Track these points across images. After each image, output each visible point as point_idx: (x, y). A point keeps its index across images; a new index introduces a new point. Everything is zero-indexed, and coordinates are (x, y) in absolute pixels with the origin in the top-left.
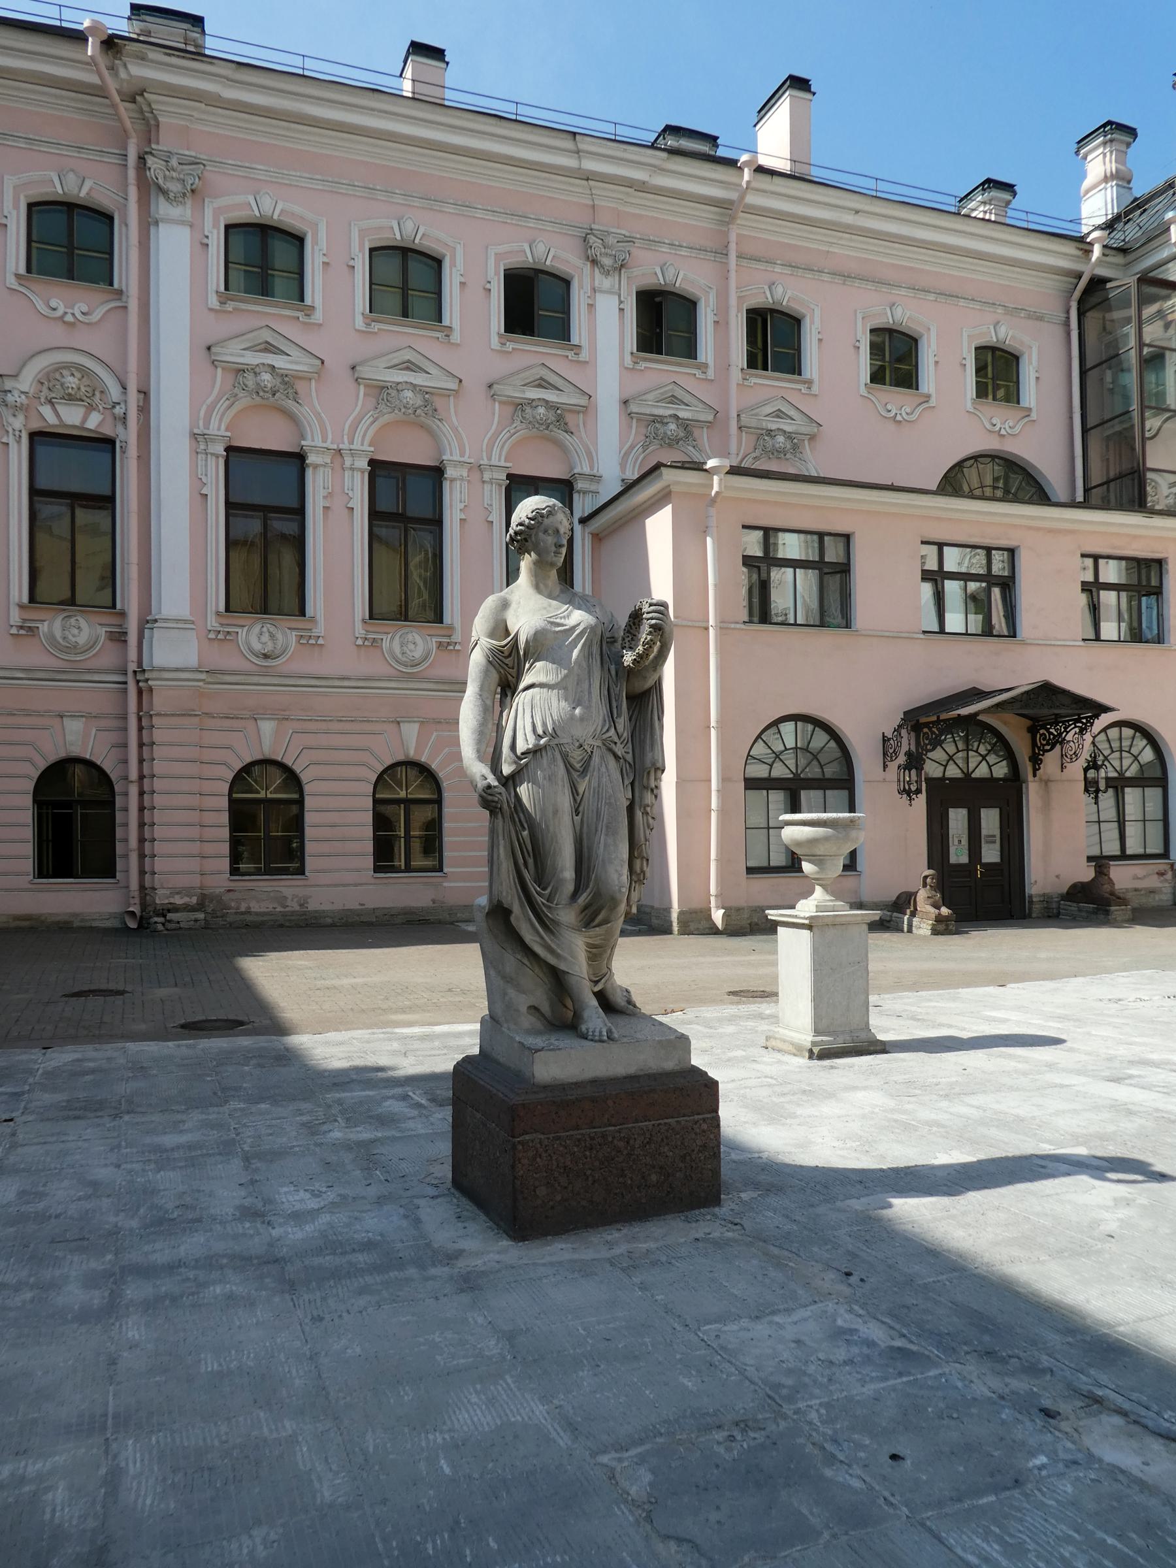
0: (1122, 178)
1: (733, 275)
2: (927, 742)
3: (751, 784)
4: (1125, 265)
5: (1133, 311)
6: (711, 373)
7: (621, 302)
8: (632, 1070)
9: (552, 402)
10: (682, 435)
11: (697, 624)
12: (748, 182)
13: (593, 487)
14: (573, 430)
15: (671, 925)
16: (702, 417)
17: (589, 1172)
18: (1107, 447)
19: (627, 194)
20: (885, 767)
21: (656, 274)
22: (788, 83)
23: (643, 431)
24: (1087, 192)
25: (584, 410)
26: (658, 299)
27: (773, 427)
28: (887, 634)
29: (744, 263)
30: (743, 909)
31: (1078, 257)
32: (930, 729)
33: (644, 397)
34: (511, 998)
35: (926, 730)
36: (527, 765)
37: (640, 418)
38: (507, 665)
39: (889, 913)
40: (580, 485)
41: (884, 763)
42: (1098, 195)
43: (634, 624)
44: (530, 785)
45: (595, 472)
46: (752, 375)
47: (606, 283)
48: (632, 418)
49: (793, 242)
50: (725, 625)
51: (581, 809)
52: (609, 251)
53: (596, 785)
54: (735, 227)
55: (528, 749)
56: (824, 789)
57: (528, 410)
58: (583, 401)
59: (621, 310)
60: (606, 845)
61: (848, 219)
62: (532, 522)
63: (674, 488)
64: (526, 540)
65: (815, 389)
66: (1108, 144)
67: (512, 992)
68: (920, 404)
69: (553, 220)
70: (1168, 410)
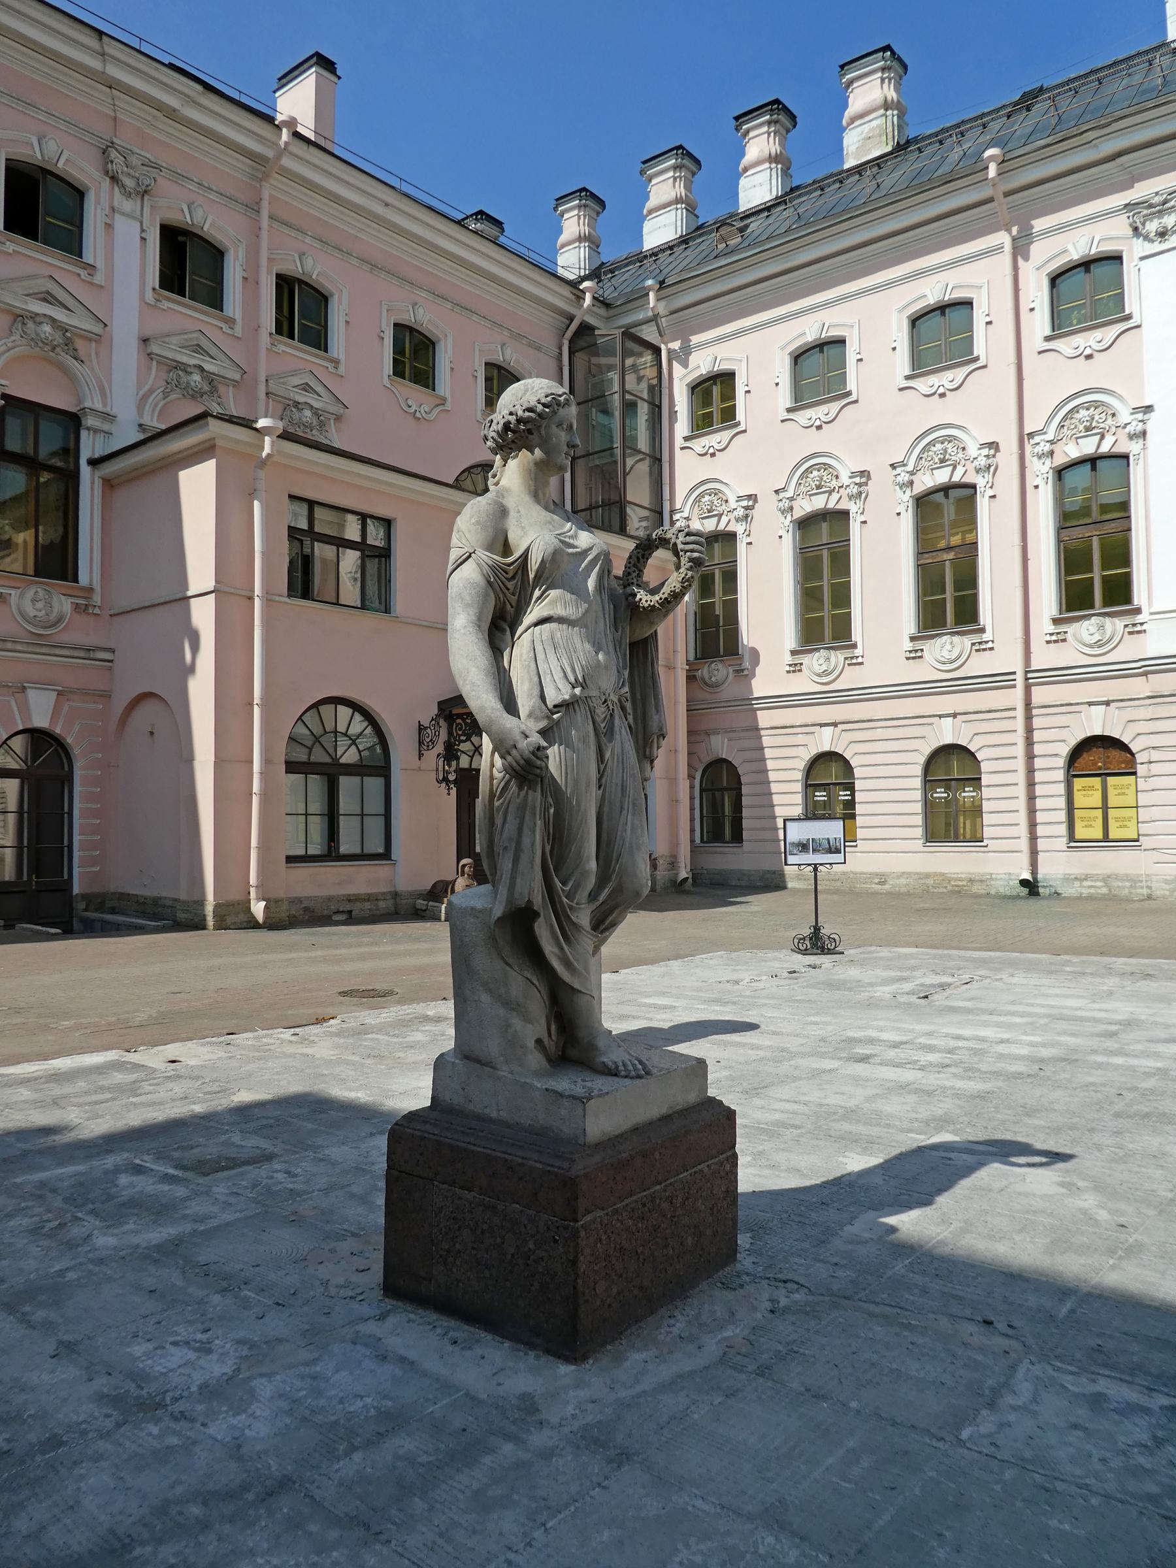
0: (592, 241)
1: (264, 235)
2: (460, 733)
3: (292, 767)
4: (607, 318)
5: (617, 360)
6: (238, 331)
7: (143, 231)
8: (664, 1110)
9: (60, 322)
10: (206, 388)
11: (240, 592)
12: (286, 143)
13: (106, 427)
14: (83, 359)
15: (205, 919)
16: (230, 375)
17: (640, 1250)
18: (591, 476)
19: (154, 117)
20: (420, 755)
21: (182, 210)
22: (315, 59)
23: (164, 375)
24: (563, 246)
25: (97, 339)
26: (181, 239)
27: (301, 399)
28: (424, 623)
29: (276, 225)
30: (282, 900)
31: (572, 300)
32: (464, 720)
33: (166, 339)
34: (516, 1031)
35: (459, 721)
36: (558, 722)
37: (162, 361)
38: (508, 589)
39: (425, 902)
40: (90, 421)
41: (420, 751)
42: (572, 251)
43: (643, 557)
44: (562, 747)
45: (108, 410)
46: (281, 342)
47: (128, 205)
48: (152, 359)
49: (325, 218)
50: (270, 597)
51: (603, 781)
52: (132, 172)
53: (620, 751)
54: (268, 185)
55: (564, 701)
56: (362, 775)
57: (30, 324)
58: (97, 329)
59: (143, 239)
60: (633, 829)
61: (379, 209)
62: (547, 410)
63: (218, 442)
64: (530, 432)
65: (342, 370)
66: (583, 208)
67: (517, 1022)
68: (437, 405)
69: (67, 119)
70: (640, 452)
